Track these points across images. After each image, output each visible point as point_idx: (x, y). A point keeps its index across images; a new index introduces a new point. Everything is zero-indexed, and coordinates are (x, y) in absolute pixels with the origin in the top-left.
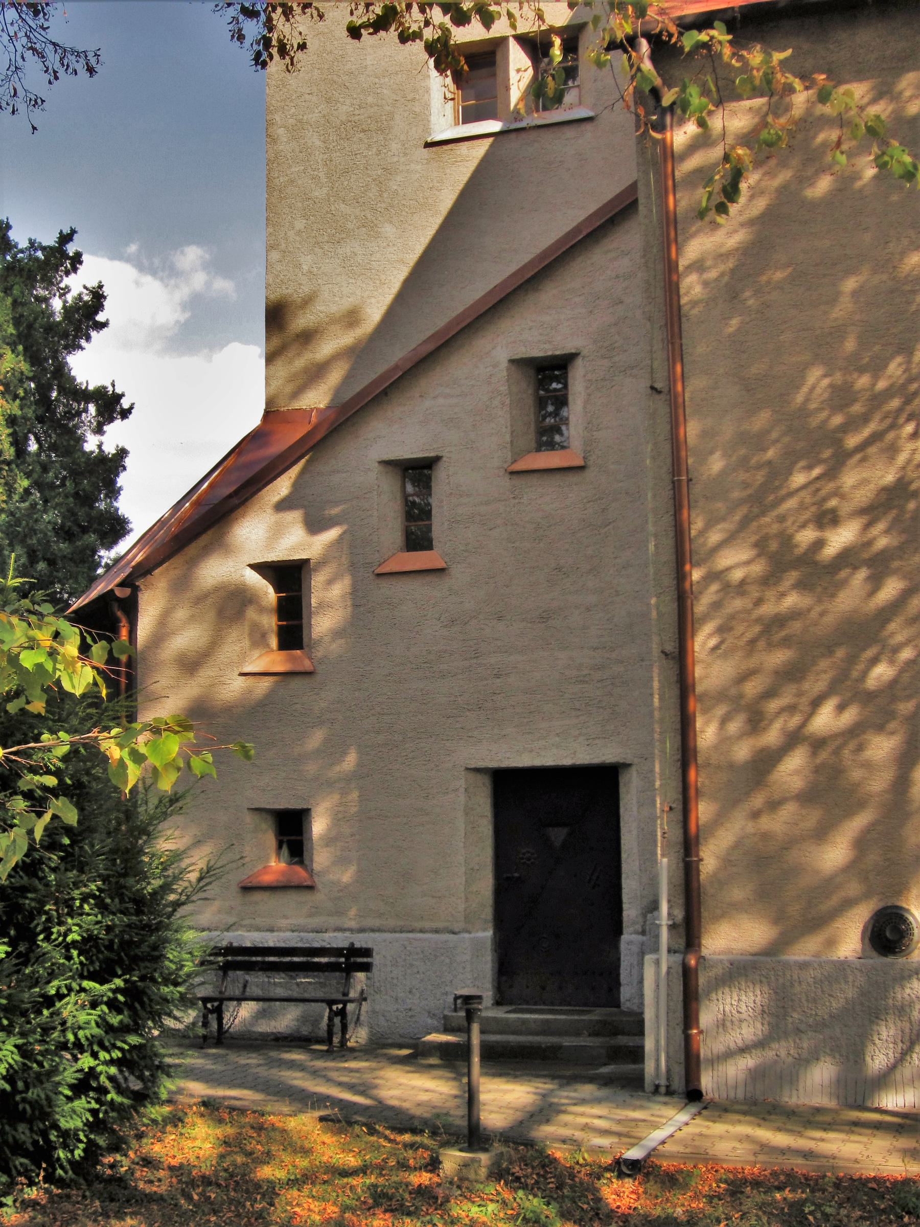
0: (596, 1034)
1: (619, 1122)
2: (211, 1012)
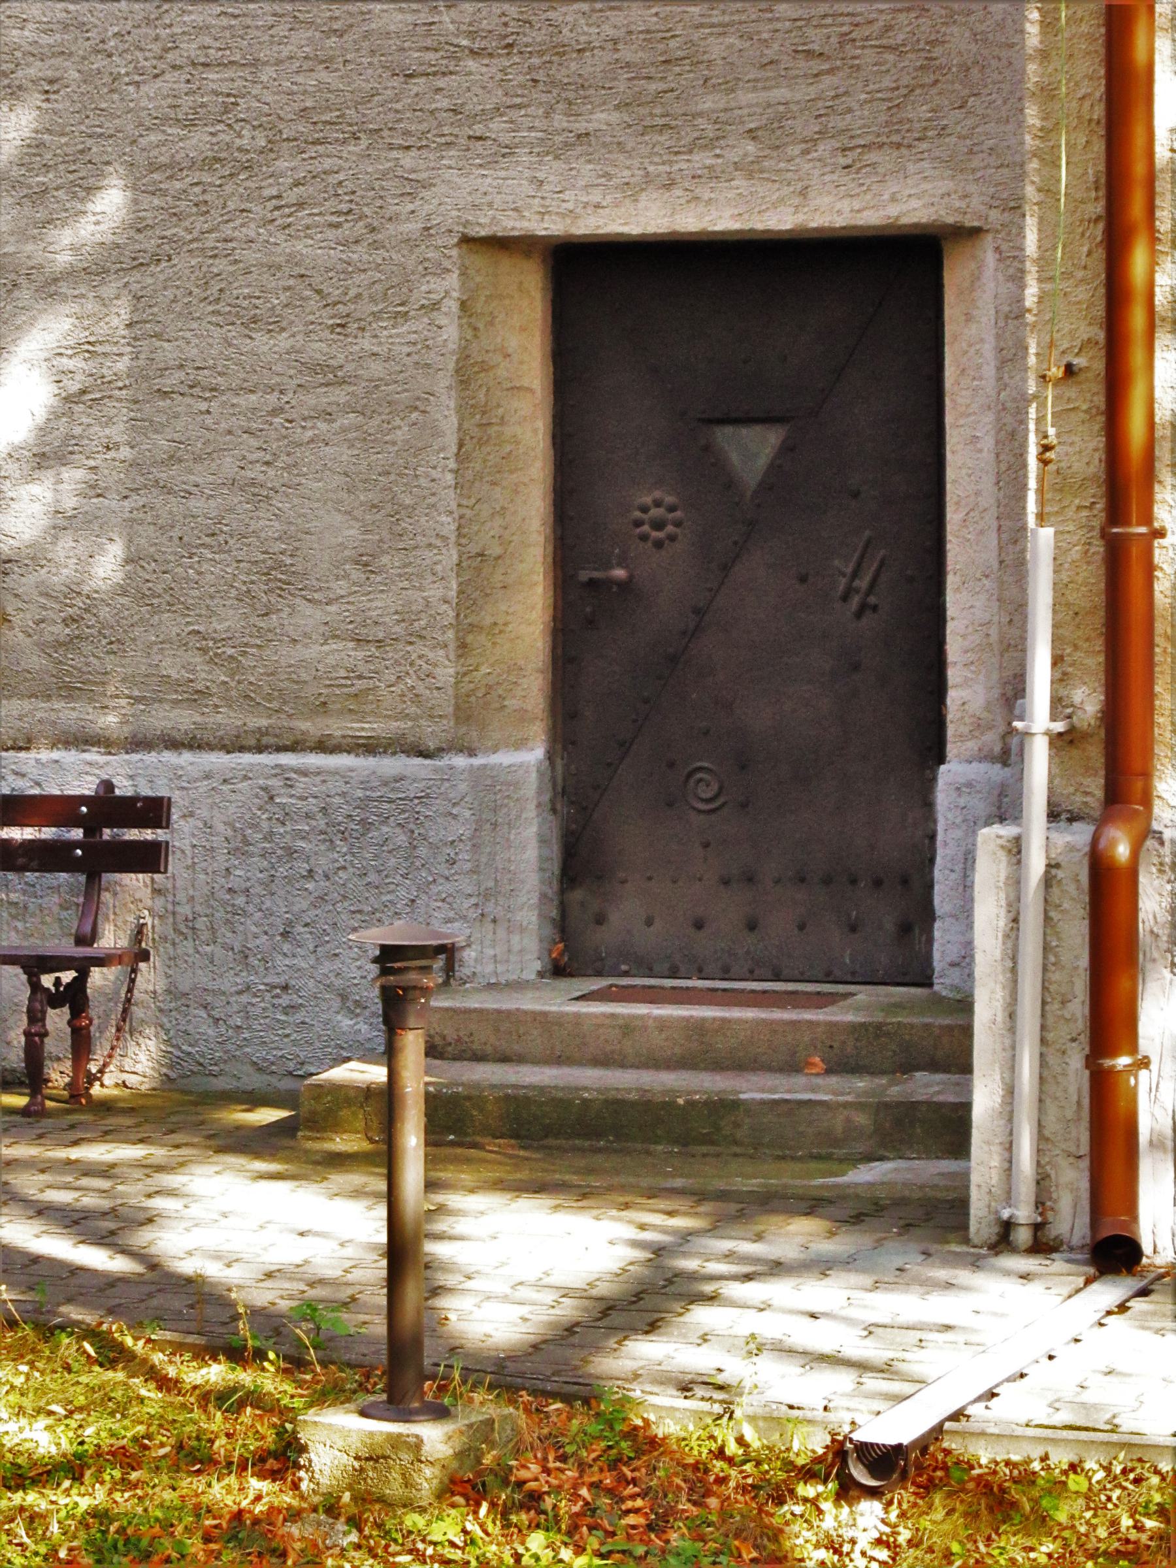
0: (840, 1066)
1: (870, 1330)
2: (55, 1000)
